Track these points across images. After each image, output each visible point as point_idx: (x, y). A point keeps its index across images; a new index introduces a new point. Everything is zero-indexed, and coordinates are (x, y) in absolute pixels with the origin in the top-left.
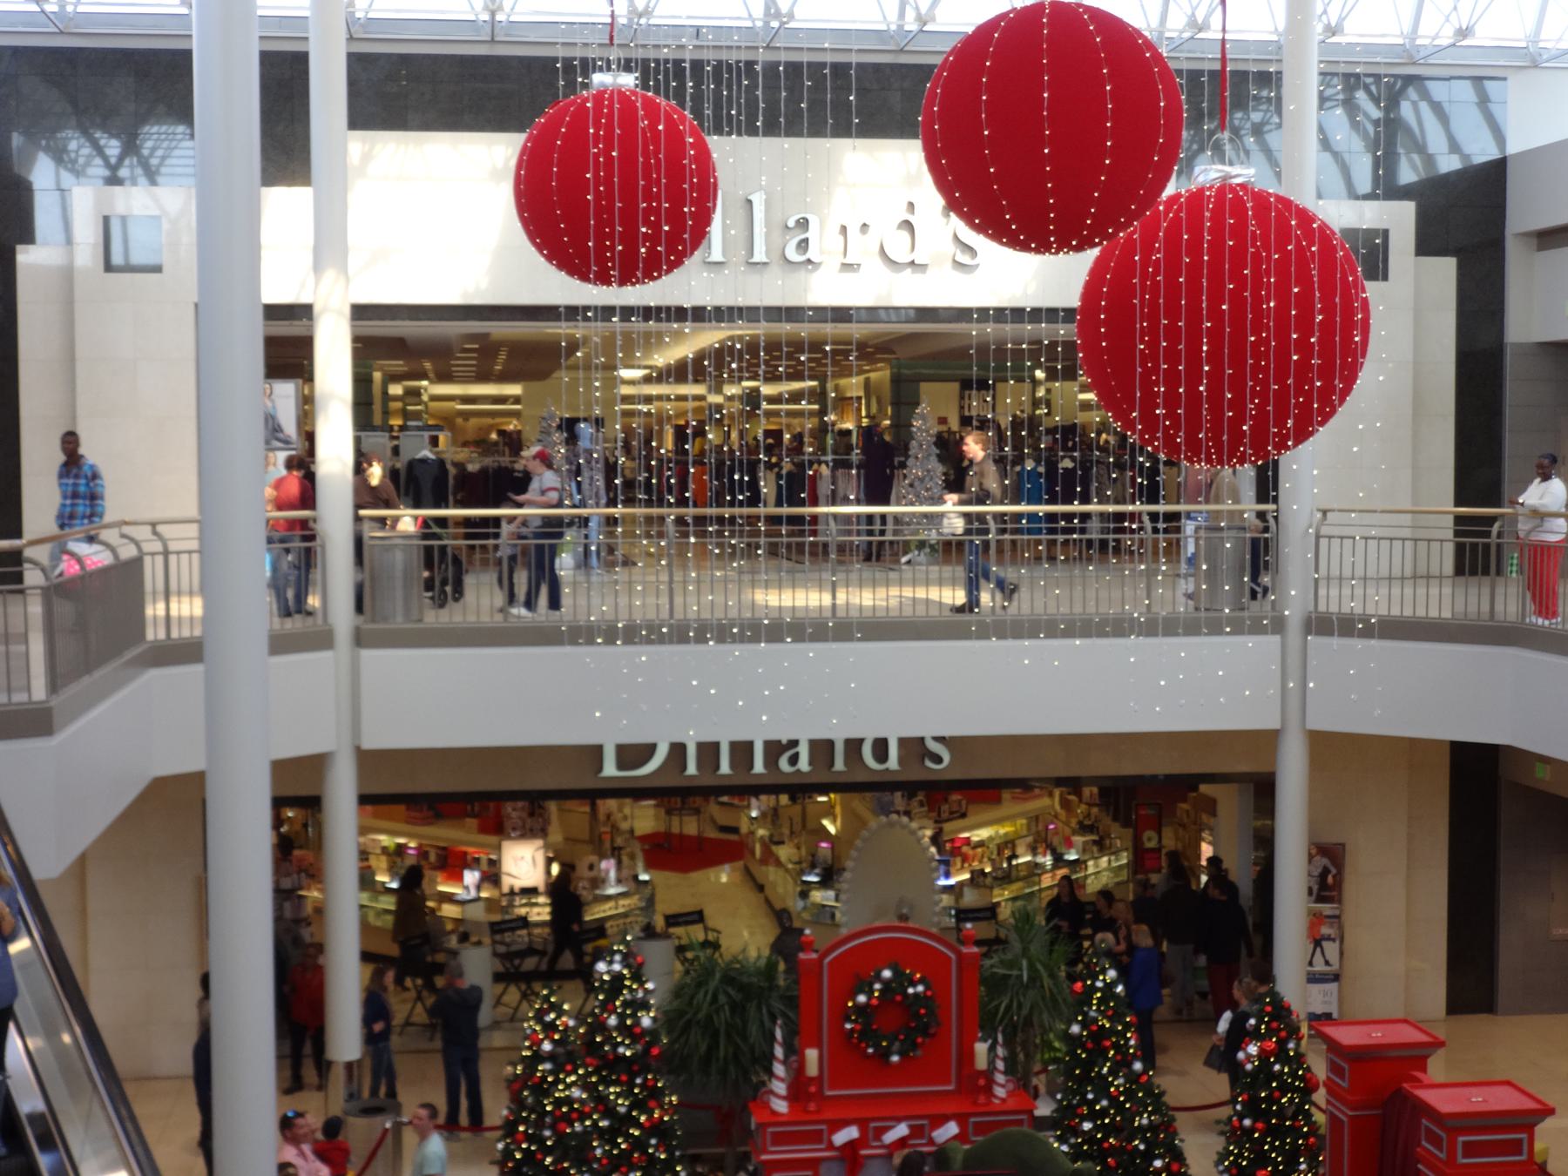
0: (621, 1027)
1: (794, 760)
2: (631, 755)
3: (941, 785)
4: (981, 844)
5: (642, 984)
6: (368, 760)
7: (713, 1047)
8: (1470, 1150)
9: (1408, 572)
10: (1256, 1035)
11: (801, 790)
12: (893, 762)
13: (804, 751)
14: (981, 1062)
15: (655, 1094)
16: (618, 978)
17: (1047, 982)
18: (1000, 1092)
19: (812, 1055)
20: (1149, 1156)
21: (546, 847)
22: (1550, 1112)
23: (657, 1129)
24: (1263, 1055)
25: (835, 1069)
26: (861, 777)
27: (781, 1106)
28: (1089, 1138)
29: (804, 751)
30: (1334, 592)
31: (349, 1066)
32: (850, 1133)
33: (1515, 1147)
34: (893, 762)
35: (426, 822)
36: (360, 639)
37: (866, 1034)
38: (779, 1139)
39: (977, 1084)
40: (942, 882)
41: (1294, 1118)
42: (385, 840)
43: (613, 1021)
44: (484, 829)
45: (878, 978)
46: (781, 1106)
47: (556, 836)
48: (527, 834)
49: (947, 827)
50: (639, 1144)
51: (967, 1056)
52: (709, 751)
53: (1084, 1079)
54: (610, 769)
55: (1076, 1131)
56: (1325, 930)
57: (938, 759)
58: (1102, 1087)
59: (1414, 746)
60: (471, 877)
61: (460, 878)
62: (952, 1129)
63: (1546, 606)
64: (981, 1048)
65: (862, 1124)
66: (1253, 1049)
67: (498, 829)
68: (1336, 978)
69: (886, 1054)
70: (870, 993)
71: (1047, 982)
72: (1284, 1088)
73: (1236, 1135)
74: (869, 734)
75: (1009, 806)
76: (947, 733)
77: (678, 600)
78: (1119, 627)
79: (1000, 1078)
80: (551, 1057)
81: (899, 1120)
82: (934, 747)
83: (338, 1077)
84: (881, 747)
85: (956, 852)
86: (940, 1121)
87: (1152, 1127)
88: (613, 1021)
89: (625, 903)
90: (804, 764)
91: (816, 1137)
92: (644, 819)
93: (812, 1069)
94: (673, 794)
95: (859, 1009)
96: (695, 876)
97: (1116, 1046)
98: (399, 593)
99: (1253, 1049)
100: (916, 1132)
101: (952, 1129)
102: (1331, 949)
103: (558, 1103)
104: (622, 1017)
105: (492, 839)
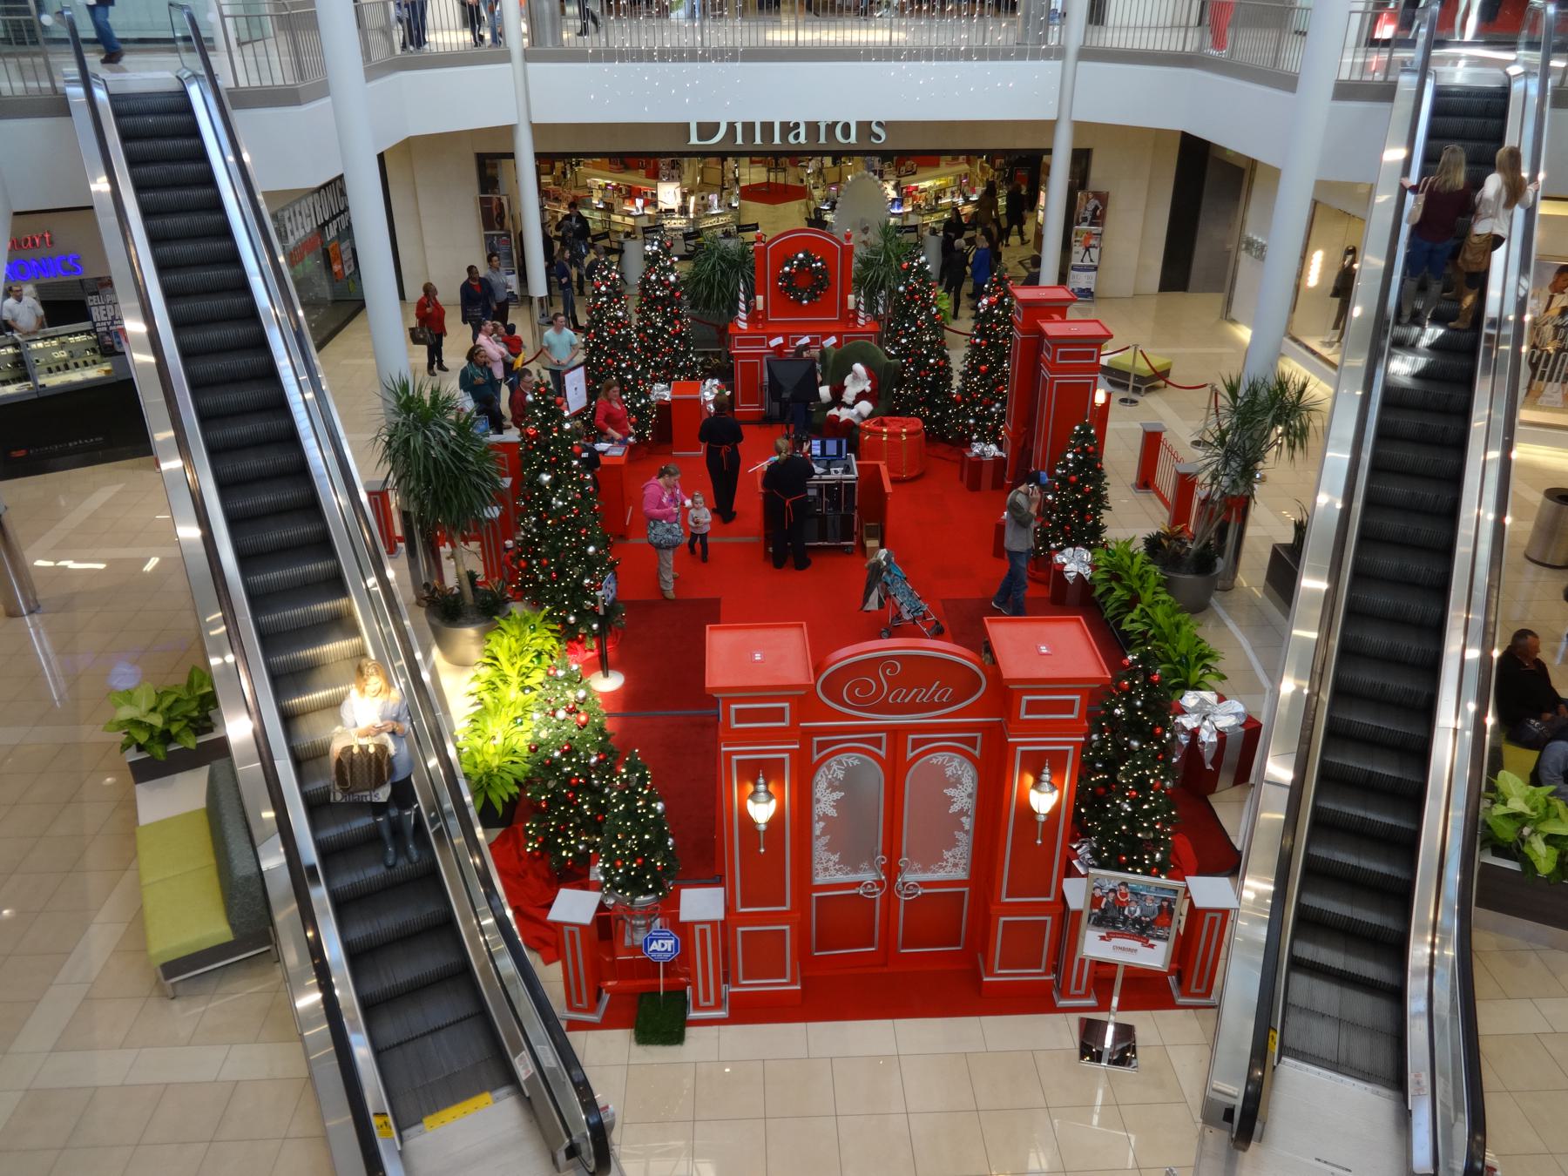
0: (658, 281)
1: (797, 136)
2: (707, 130)
3: (904, 151)
4: (924, 190)
5: (669, 258)
6: (538, 130)
7: (710, 295)
8: (1064, 356)
9: (1168, 24)
10: (988, 294)
11: (838, 155)
12: (853, 139)
13: (802, 130)
14: (851, 306)
15: (678, 316)
16: (656, 254)
17: (894, 262)
18: (861, 322)
19: (760, 298)
20: (928, 357)
21: (682, 186)
22: (1111, 337)
23: (677, 335)
24: (990, 304)
25: (776, 306)
26: (835, 148)
27: (743, 326)
28: (905, 347)
29: (802, 130)
30: (1116, 35)
31: (541, 299)
32: (780, 340)
33: (1090, 355)
34: (853, 139)
35: (620, 171)
36: (528, 56)
37: (788, 288)
38: (741, 342)
39: (850, 317)
40: (895, 211)
41: (1004, 338)
42: (601, 182)
43: (653, 277)
44: (648, 176)
45: (796, 258)
46: (743, 326)
47: (687, 180)
48: (671, 179)
49: (903, 180)
50: (669, 343)
51: (844, 302)
52: (749, 127)
53: (905, 316)
54: (694, 140)
55: (898, 343)
56: (1092, 242)
57: (879, 138)
58: (914, 320)
59: (1160, 133)
60: (639, 202)
61: (634, 203)
62: (833, 340)
63: (1219, 43)
64: (851, 298)
65: (785, 336)
66: (985, 301)
67: (655, 175)
68: (1096, 269)
69: (801, 300)
70: (791, 266)
71: (894, 262)
72: (998, 324)
73: (974, 346)
74: (758, 119)
75: (944, 168)
76: (883, 120)
77: (706, 36)
78: (953, 55)
79: (862, 314)
80: (606, 294)
81: (778, 335)
82: (876, 129)
83: (536, 304)
84: (846, 126)
85: (909, 194)
86: (827, 336)
87: (931, 342)
88: (653, 277)
89: (722, 220)
90: (802, 139)
91: (761, 342)
92: (754, 175)
93: (760, 307)
94: (773, 158)
95: (787, 275)
96: (781, 206)
97: (922, 299)
98: (548, 28)
99: (985, 301)
100: (814, 341)
101: (833, 340)
102: (1094, 252)
103: (610, 319)
104: (658, 276)
105: (652, 182)
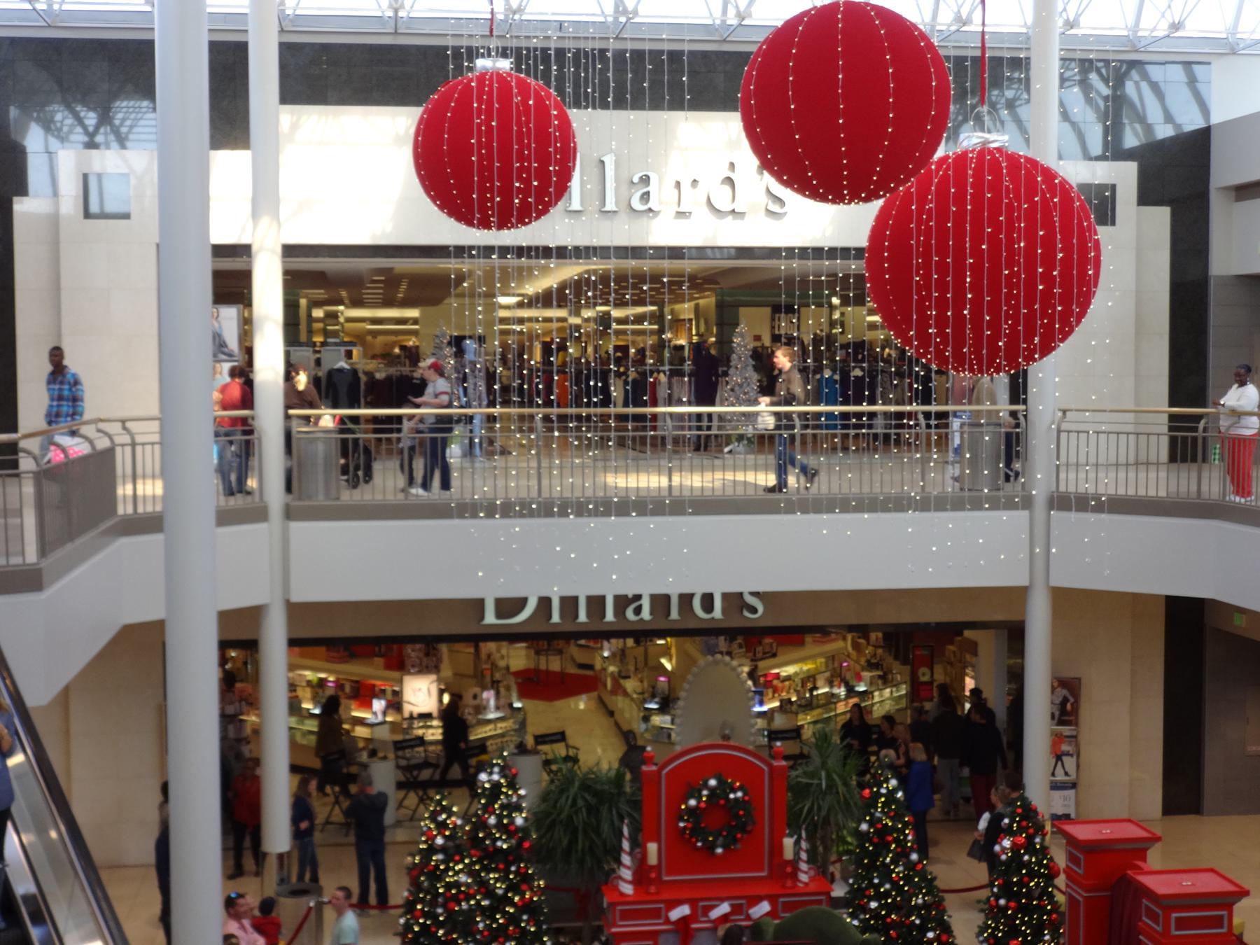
0: (499, 825)
1: (638, 611)
2: (507, 607)
3: (756, 630)
4: (788, 678)
5: (516, 790)
6: (296, 611)
7: (573, 842)
8: (1181, 924)
9: (1132, 460)
10: (1009, 832)
11: (643, 635)
12: (718, 612)
13: (646, 604)
14: (789, 854)
15: (526, 879)
16: (496, 786)
17: (841, 789)
18: (804, 878)
19: (652, 847)
20: (923, 929)
21: (439, 680)
22: (1246, 893)
23: (528, 907)
24: (1015, 848)
25: (671, 859)
26: (692, 625)
27: (628, 889)
28: (875, 914)
29: (646, 604)
30: (1072, 476)
31: (281, 857)
32: (683, 911)
33: (1218, 922)
34: (718, 612)
35: (342, 660)
36: (290, 514)
37: (696, 831)
38: (626, 915)
39: (785, 871)
40: (757, 709)
41: (1040, 898)
42: (309, 675)
43: (492, 820)
44: (389, 667)
45: (706, 786)
46: (628, 889)
47: (447, 672)
48: (423, 670)
49: (761, 664)
50: (513, 919)
51: (777, 848)
52: (570, 604)
53: (871, 867)
54: (490, 618)
55: (865, 909)
56: (1065, 748)
57: (754, 610)
58: (886, 873)
59: (1136, 600)
60: (378, 705)
61: (370, 706)
62: (765, 907)
63: (1242, 487)
64: (788, 842)
65: (693, 903)
66: (1007, 843)
67: (400, 666)
68: (1074, 785)
69: (712, 847)
70: (699, 798)
71: (841, 789)
72: (1032, 875)
73: (993, 912)
75: (811, 648)
76: (761, 589)
77: (545, 482)
78: (899, 504)
79: (804, 866)
80: (443, 849)
81: (723, 900)
82: (750, 600)
83: (271, 866)
84: (708, 600)
85: (768, 684)
86: (755, 901)
87: (925, 906)
88: (492, 820)
89: (502, 726)
90: (646, 614)
91: (655, 914)
92: (517, 658)
93: (653, 859)
94: (541, 638)
95: (691, 811)
96: (559, 704)
97: (896, 841)
98: (321, 477)
99: (1007, 843)
100: (736, 909)
101: (765, 907)
102: (1070, 762)
103: (449, 886)
104: (500, 817)
105: (396, 674)
